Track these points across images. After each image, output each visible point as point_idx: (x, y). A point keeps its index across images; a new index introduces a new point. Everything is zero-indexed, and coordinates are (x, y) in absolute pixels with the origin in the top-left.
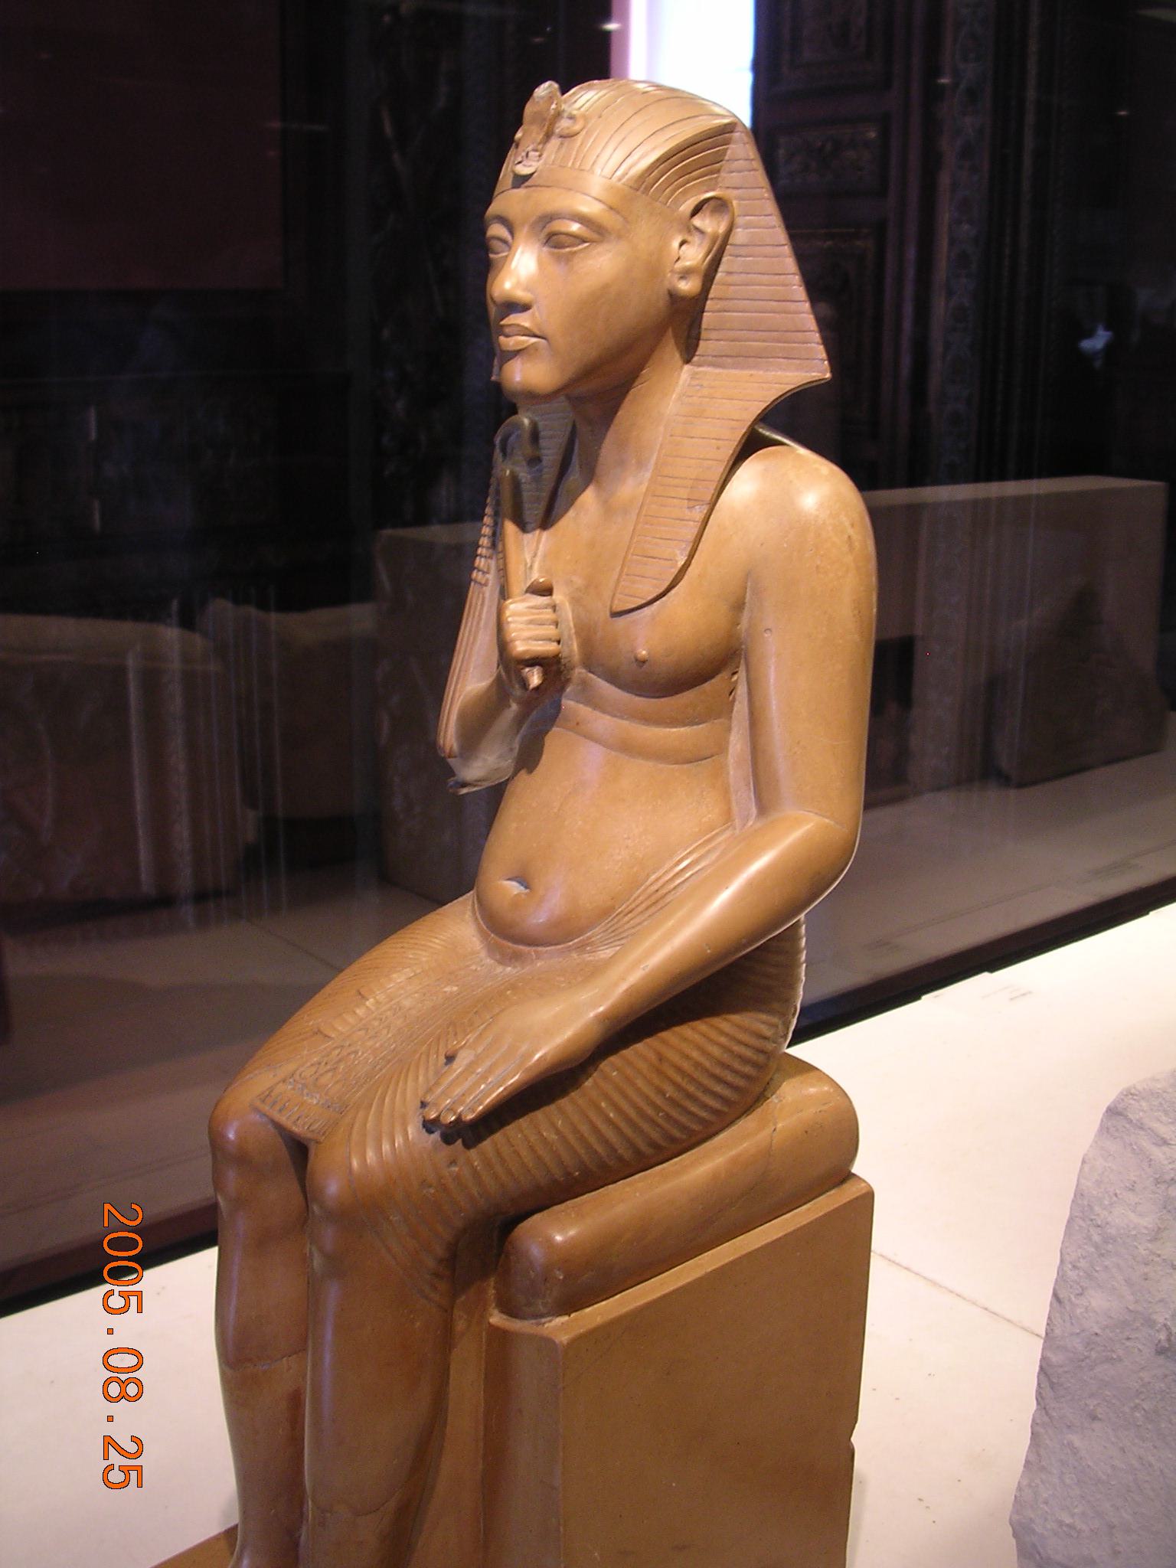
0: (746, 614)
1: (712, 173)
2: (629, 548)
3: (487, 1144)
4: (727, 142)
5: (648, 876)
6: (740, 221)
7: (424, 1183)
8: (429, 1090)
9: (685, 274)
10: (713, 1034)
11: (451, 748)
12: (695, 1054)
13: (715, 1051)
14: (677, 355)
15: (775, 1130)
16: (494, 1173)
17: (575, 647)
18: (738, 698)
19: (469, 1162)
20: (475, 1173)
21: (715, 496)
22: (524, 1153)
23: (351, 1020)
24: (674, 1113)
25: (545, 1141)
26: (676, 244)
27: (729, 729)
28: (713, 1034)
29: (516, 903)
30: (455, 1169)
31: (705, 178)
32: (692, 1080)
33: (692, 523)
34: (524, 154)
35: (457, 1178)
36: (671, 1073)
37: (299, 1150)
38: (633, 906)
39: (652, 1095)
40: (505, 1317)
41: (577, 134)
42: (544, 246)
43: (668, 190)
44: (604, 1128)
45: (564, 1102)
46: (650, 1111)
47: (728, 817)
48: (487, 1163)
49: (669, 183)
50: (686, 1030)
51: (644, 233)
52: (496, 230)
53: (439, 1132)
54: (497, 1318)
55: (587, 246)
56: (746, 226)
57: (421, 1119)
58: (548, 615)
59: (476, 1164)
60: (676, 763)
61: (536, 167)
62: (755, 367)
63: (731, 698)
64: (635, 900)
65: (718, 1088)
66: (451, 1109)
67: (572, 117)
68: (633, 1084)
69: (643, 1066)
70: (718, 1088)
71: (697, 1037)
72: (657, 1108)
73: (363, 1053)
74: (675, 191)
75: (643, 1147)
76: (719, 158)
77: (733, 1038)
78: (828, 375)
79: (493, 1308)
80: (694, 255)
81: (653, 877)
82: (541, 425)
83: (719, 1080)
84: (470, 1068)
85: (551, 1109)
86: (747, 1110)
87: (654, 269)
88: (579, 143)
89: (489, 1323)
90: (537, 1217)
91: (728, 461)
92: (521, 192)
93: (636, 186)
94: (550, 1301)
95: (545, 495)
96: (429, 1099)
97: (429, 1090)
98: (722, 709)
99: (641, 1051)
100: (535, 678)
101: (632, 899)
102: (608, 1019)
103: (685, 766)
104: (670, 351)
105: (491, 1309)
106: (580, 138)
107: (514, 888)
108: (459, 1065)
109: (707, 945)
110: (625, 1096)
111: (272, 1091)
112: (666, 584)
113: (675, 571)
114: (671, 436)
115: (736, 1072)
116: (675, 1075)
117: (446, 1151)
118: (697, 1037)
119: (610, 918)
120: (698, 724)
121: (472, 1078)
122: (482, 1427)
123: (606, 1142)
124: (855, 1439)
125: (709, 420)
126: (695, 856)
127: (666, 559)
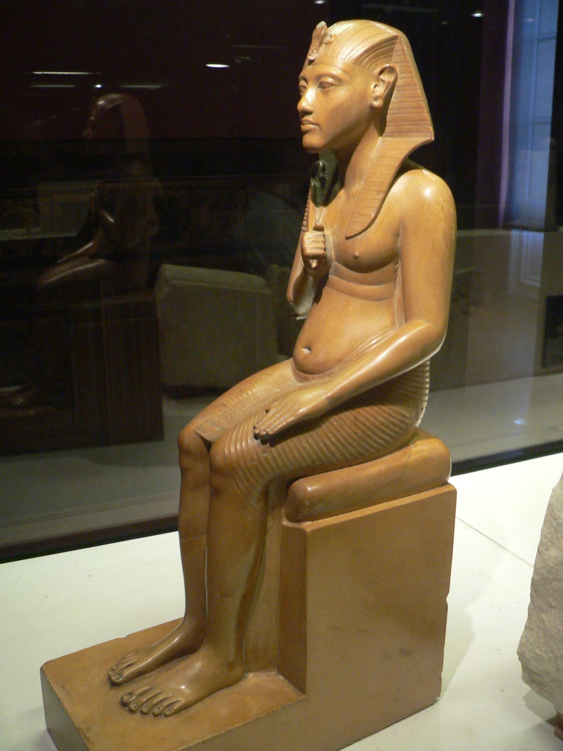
0: (400, 239)
1: (389, 56)
2: (354, 211)
3: (279, 447)
4: (395, 44)
5: (358, 346)
6: (399, 76)
7: (252, 459)
8: (258, 423)
9: (376, 98)
10: (380, 412)
11: (291, 297)
12: (372, 419)
13: (381, 419)
14: (376, 133)
17: (333, 253)
18: (398, 274)
19: (271, 452)
22: (295, 451)
23: (236, 400)
24: (363, 444)
26: (372, 86)
27: (395, 288)
28: (380, 412)
29: (306, 357)
30: (266, 455)
32: (370, 429)
37: (208, 445)
39: (352, 434)
40: (289, 522)
41: (333, 42)
42: (318, 88)
46: (350, 440)
47: (393, 324)
48: (279, 455)
49: (370, 61)
50: (368, 409)
51: (359, 82)
52: (302, 83)
54: (285, 523)
56: (403, 78)
57: (253, 434)
58: (322, 239)
61: (316, 56)
62: (406, 136)
63: (395, 274)
65: (383, 435)
66: (265, 430)
67: (331, 36)
68: (344, 429)
69: (349, 422)
70: (383, 435)
71: (372, 412)
72: (354, 440)
73: (239, 412)
75: (349, 457)
76: (391, 50)
77: (389, 414)
78: (433, 138)
80: (380, 90)
81: (360, 347)
82: (326, 165)
83: (383, 431)
84: (274, 415)
85: (307, 435)
86: (399, 448)
87: (363, 96)
88: (333, 46)
90: (301, 480)
92: (311, 67)
96: (257, 426)
97: (258, 423)
98: (393, 279)
99: (348, 416)
100: (314, 264)
104: (373, 131)
106: (333, 45)
107: (306, 351)
108: (270, 414)
110: (339, 432)
112: (366, 225)
113: (370, 220)
115: (391, 430)
117: (263, 447)
118: (372, 412)
121: (275, 419)
123: (331, 451)
124: (450, 599)
126: (378, 339)
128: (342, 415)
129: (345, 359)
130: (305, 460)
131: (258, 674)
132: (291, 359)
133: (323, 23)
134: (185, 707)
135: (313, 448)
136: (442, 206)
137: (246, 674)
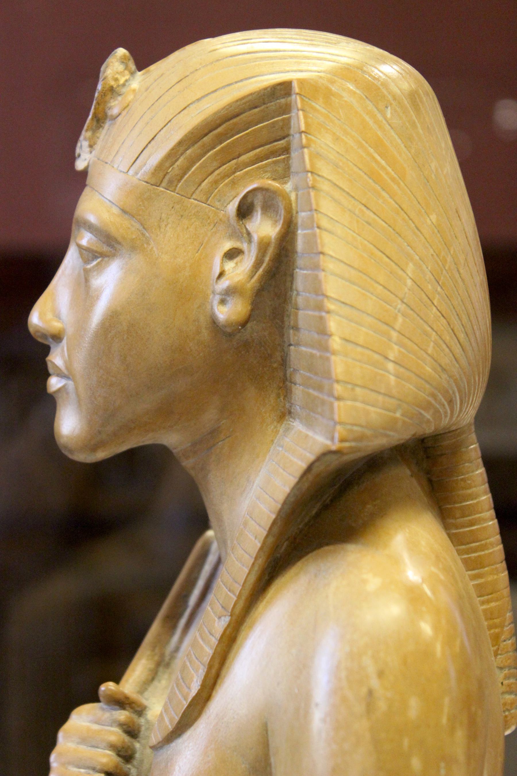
4: (287, 109)
74: (216, 182)
93: (153, 181)
136: (370, 693)
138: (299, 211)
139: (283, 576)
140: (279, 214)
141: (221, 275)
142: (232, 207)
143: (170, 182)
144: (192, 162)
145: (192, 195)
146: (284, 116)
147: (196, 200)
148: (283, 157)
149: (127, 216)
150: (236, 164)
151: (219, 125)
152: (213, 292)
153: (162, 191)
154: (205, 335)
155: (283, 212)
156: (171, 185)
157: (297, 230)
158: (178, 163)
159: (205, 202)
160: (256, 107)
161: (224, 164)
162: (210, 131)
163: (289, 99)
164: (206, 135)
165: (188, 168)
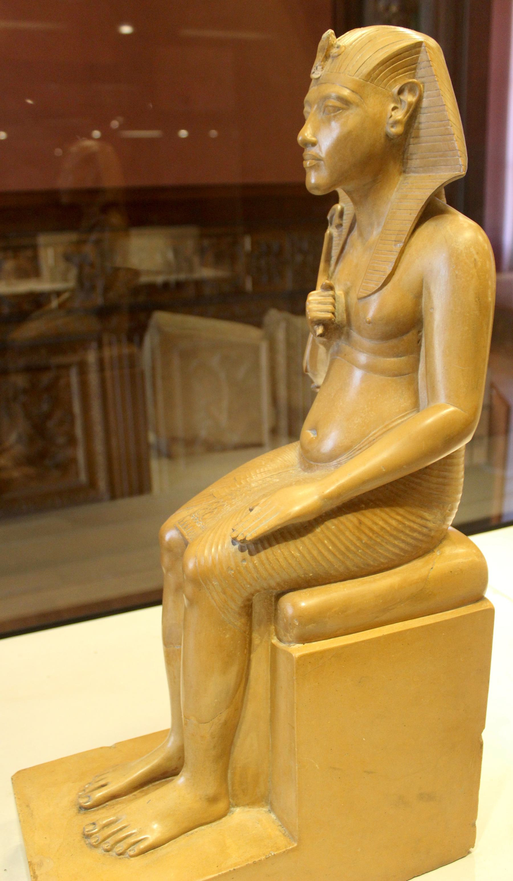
3: (262, 554)
4: (418, 53)
5: (370, 432)
9: (396, 123)
15: (432, 568)
16: (265, 568)
20: (255, 567)
21: (407, 240)
22: (281, 560)
25: (293, 556)
29: (311, 442)
30: (245, 563)
31: (407, 73)
33: (395, 253)
34: (315, 68)
35: (246, 567)
36: (367, 531)
38: (362, 446)
39: (355, 540)
43: (385, 80)
44: (326, 553)
45: (305, 539)
46: (353, 548)
49: (386, 76)
53: (238, 545)
54: (275, 641)
55: (341, 112)
56: (428, 97)
58: (331, 300)
59: (255, 562)
60: (390, 376)
63: (419, 344)
64: (362, 444)
69: (350, 525)
73: (227, 506)
74: (389, 81)
79: (274, 636)
80: (399, 115)
81: (373, 433)
82: (345, 209)
89: (272, 643)
91: (414, 221)
93: (366, 79)
94: (293, 635)
95: (341, 242)
101: (361, 443)
102: (326, 499)
103: (395, 378)
105: (272, 636)
109: (383, 467)
110: (339, 540)
111: (184, 519)
113: (385, 277)
114: (392, 209)
116: (368, 532)
117: (240, 554)
119: (350, 451)
120: (401, 357)
122: (269, 693)
124: (485, 735)
125: (408, 200)
127: (382, 271)
128: (343, 519)
129: (355, 447)
130: (295, 570)
131: (246, 809)
132: (299, 442)
133: (330, 31)
134: (153, 847)
135: (303, 556)
136: (475, 260)
137: (232, 809)
138: (424, 91)
139: (420, 228)
140: (335, 114)
141: (391, 116)
142: (396, 89)
143: (372, 80)
144: (381, 72)
145: (380, 85)
146: (417, 55)
147: (381, 87)
148: (413, 71)
149: (354, 93)
150: (397, 74)
151: (394, 58)
152: (387, 123)
153: (369, 84)
154: (383, 140)
155: (418, 93)
156: (372, 81)
157: (423, 98)
158: (376, 72)
159: (384, 87)
160: (407, 51)
161: (392, 73)
162: (390, 60)
163: (420, 48)
164: (388, 61)
165: (379, 75)
